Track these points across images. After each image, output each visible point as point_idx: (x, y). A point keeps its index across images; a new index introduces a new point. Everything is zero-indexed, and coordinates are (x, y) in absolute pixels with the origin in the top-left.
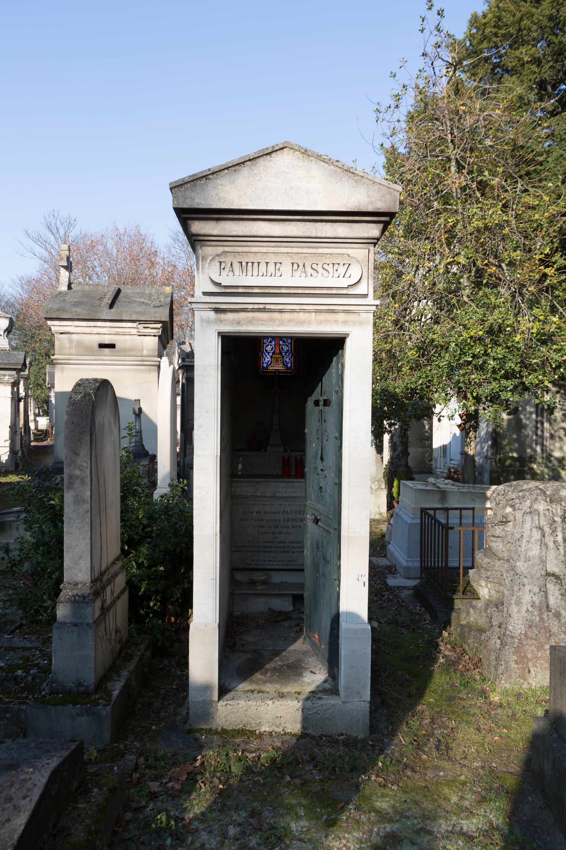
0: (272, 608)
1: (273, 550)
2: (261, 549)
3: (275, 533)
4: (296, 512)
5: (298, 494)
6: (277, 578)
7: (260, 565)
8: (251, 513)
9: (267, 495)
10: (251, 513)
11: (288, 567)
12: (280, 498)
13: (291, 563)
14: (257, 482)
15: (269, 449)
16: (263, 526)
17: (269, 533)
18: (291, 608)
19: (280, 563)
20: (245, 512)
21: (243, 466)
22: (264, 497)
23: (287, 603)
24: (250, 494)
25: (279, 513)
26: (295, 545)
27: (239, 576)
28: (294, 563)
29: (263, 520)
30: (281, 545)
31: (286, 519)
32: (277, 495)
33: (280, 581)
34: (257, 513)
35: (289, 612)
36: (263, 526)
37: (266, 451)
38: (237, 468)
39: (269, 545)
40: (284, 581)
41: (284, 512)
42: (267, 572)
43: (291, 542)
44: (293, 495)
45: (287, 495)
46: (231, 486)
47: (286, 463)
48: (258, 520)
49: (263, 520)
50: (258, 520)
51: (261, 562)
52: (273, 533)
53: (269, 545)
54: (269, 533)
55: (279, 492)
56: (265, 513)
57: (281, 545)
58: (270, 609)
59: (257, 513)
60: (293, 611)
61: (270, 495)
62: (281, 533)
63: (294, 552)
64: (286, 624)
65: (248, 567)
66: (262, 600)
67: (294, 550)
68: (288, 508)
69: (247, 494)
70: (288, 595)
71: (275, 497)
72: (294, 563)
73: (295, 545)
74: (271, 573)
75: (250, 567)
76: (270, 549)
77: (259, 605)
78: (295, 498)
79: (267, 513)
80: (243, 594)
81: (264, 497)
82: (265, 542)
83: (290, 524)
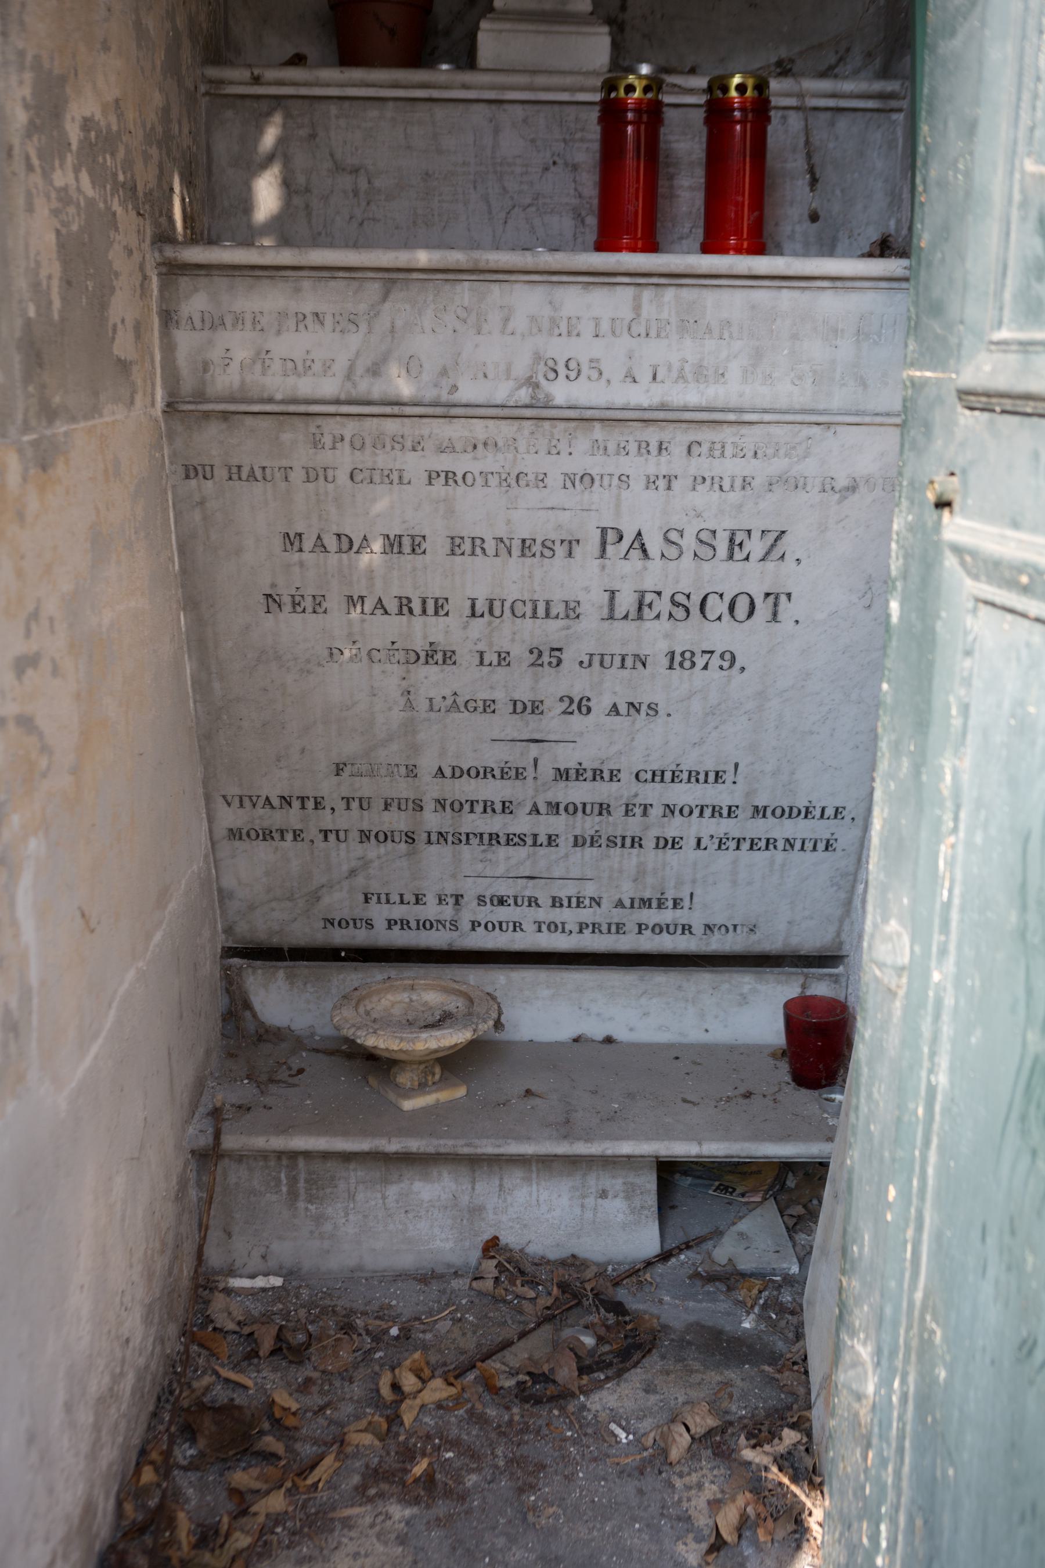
0: (508, 1238)
1: (521, 823)
2: (433, 820)
3: (536, 708)
4: (706, 541)
5: (728, 391)
6: (545, 1012)
7: (425, 925)
8: (347, 544)
9: (469, 391)
10: (347, 544)
11: (625, 943)
12: (583, 418)
13: (651, 916)
14: (393, 277)
15: (491, 42)
16: (439, 656)
17: (488, 707)
18: (646, 1240)
19: (568, 916)
20: (292, 540)
21: (287, 184)
22: (447, 410)
23: (616, 1208)
24: (329, 387)
25: (571, 545)
26: (683, 794)
27: (280, 1000)
28: (667, 916)
29: (440, 607)
30: (578, 792)
31: (626, 602)
32: (561, 392)
33: (565, 1034)
34: (393, 544)
35: (636, 1272)
36: (439, 656)
37: (468, 60)
38: (247, 205)
39: (494, 790)
40: (596, 1030)
41: (608, 537)
42: (474, 976)
43: (658, 776)
44: (691, 395)
45: (640, 395)
46: (168, 318)
47: (629, 140)
48: (405, 606)
49: (440, 607)
50: (405, 606)
51: (431, 910)
52: (517, 708)
53: (494, 790)
54: (488, 707)
55: (573, 370)
56: (455, 546)
57: (578, 792)
58: (492, 1247)
59: (393, 544)
60: (665, 1256)
61: (502, 392)
62: (583, 706)
63: (674, 844)
64: (621, 1404)
65: (340, 937)
66: (433, 1190)
67: (674, 827)
68: (643, 512)
69: (305, 387)
70: (629, 1162)
71: (537, 412)
72: (667, 916)
73: (683, 794)
74: (499, 979)
75: (360, 937)
76: (496, 824)
77: (406, 1227)
78: (710, 418)
79: (477, 545)
80: (294, 1155)
81: (447, 410)
82: (458, 772)
83: (656, 637)
